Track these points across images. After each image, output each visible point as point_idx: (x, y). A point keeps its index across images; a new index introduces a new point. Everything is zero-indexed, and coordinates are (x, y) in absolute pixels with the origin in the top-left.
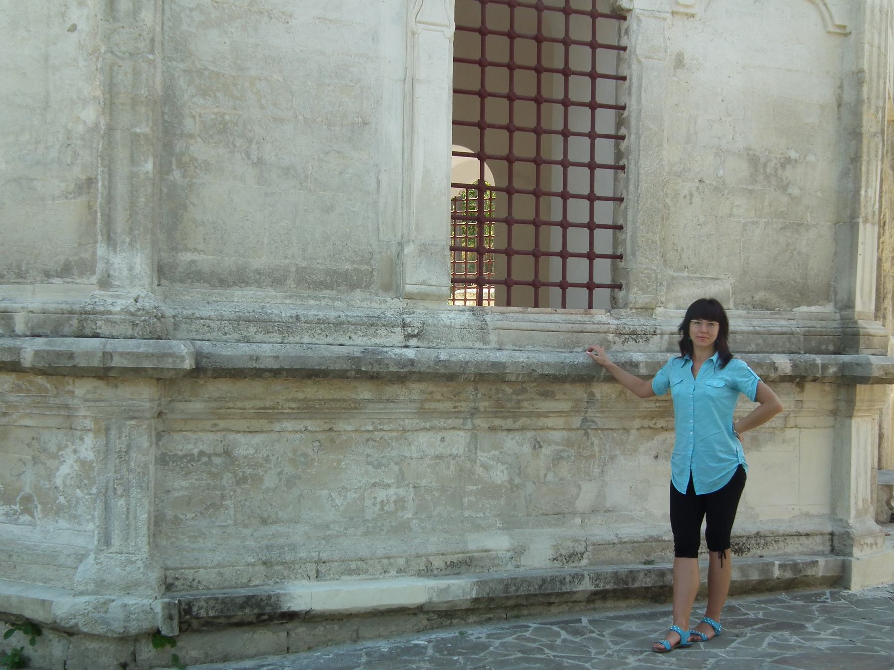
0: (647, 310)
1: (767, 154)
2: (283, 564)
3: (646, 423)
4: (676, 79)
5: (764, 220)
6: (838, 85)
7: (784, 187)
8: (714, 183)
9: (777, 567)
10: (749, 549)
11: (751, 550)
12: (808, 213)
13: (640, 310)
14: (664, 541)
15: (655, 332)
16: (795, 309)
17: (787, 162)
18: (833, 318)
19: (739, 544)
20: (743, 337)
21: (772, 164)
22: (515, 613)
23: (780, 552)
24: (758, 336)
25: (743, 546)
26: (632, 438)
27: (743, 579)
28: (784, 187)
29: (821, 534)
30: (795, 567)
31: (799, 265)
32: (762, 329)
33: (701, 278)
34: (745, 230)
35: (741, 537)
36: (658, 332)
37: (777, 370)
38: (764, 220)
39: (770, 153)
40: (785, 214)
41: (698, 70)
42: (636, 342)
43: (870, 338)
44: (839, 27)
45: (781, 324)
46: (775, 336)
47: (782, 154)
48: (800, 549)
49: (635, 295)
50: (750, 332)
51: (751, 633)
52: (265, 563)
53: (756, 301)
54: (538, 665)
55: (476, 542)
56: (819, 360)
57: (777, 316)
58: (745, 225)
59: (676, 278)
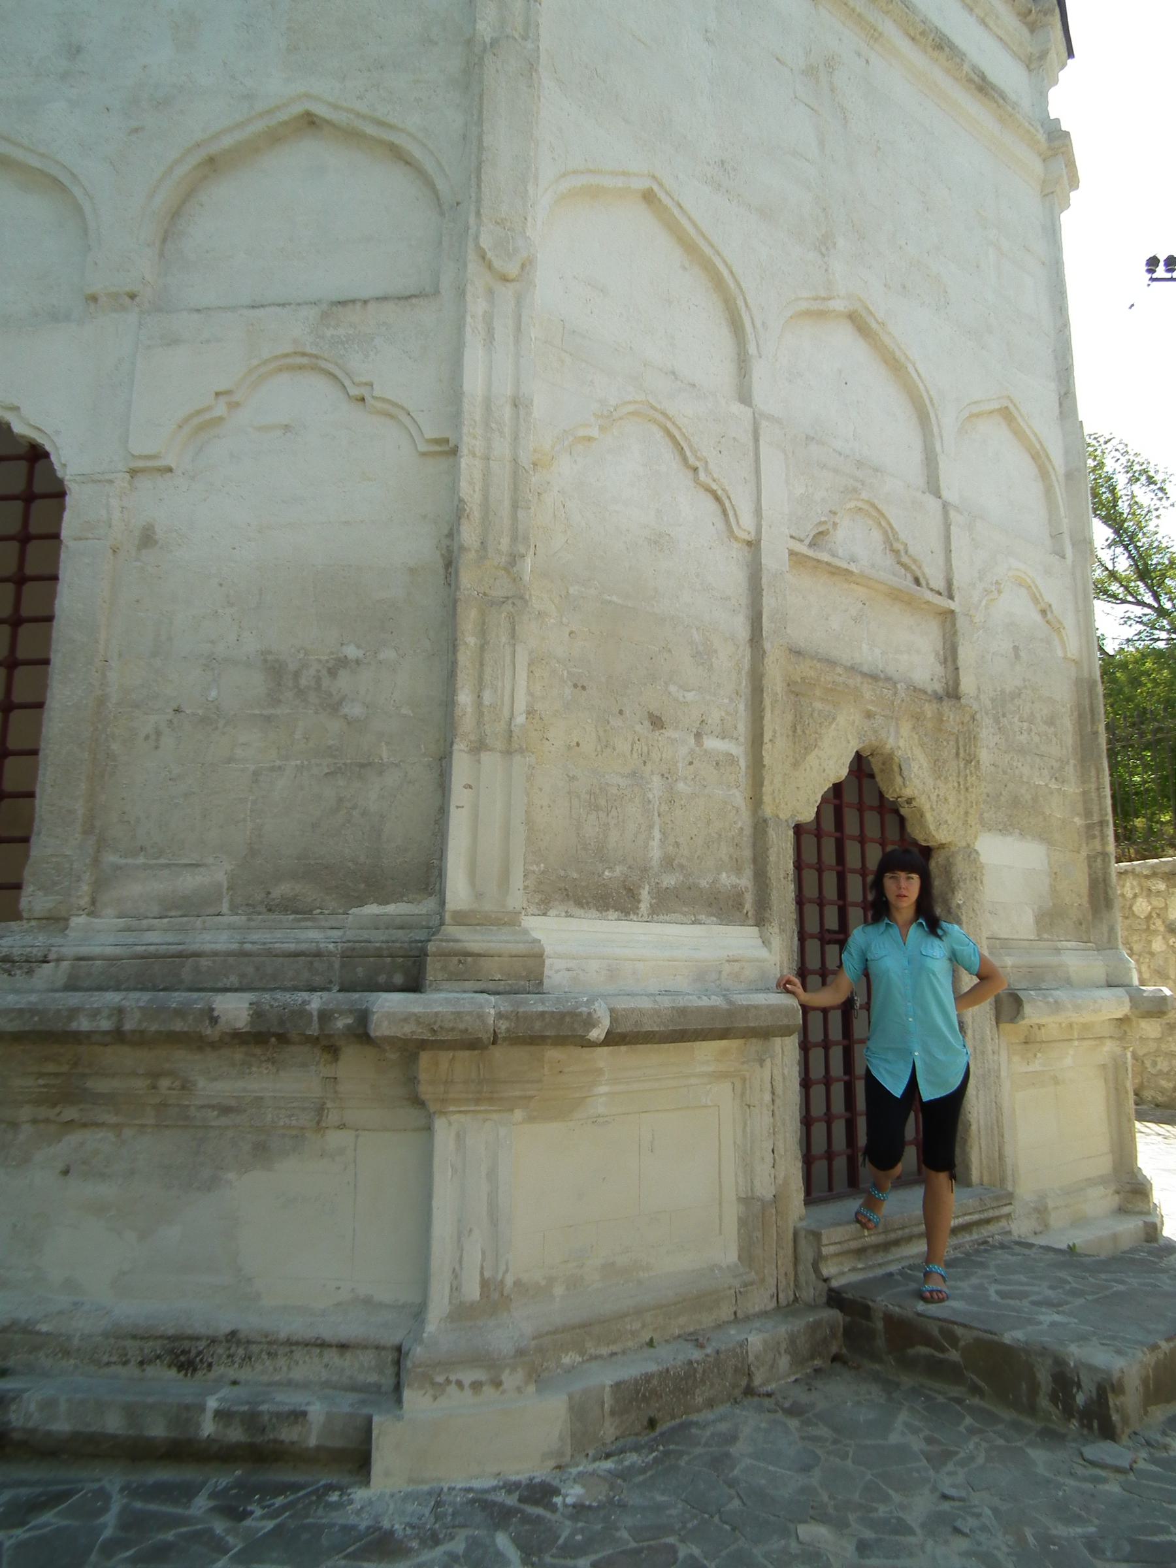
0: (56, 921)
1: (302, 656)
3: (44, 1112)
4: (139, 564)
5: (293, 763)
6: (446, 532)
7: (334, 707)
8: (200, 712)
9: (209, 1414)
10: (210, 1365)
11: (215, 1367)
12: (383, 744)
13: (44, 921)
14: (39, 1333)
15: (45, 956)
16: (354, 910)
17: (340, 664)
18: (424, 923)
19: (189, 1352)
20: (214, 962)
21: (312, 672)
23: (277, 1378)
24: (246, 960)
25: (196, 1357)
26: (22, 1137)
27: (131, 1432)
28: (334, 707)
29: (377, 1347)
30: (251, 1420)
31: (363, 833)
32: (255, 948)
33: (168, 866)
34: (256, 781)
35: (198, 1338)
36: (52, 956)
37: (216, 1022)
38: (293, 763)
39: (306, 654)
40: (337, 750)
41: (180, 545)
42: (10, 975)
43: (469, 959)
44: (437, 441)
45: (312, 936)
46: (281, 959)
47: (332, 653)
48: (324, 1375)
49: (30, 899)
50: (229, 954)
51: (903, 1434)
53: (274, 899)
56: (315, 1002)
57: (309, 924)
58: (256, 774)
59: (121, 868)
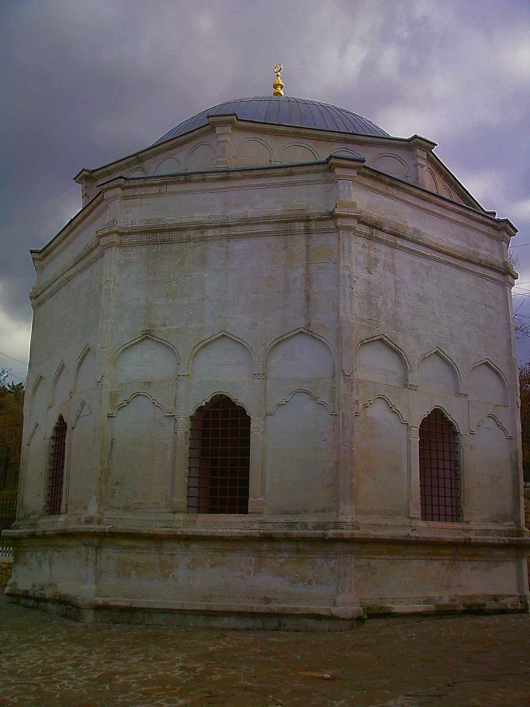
2: (385, 599)
22: (454, 616)
52: (380, 599)
54: (19, 686)
55: (430, 594)
